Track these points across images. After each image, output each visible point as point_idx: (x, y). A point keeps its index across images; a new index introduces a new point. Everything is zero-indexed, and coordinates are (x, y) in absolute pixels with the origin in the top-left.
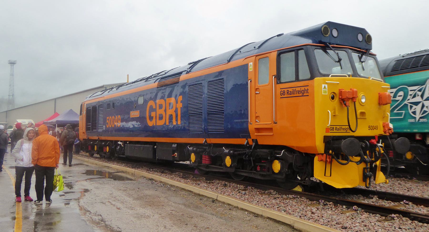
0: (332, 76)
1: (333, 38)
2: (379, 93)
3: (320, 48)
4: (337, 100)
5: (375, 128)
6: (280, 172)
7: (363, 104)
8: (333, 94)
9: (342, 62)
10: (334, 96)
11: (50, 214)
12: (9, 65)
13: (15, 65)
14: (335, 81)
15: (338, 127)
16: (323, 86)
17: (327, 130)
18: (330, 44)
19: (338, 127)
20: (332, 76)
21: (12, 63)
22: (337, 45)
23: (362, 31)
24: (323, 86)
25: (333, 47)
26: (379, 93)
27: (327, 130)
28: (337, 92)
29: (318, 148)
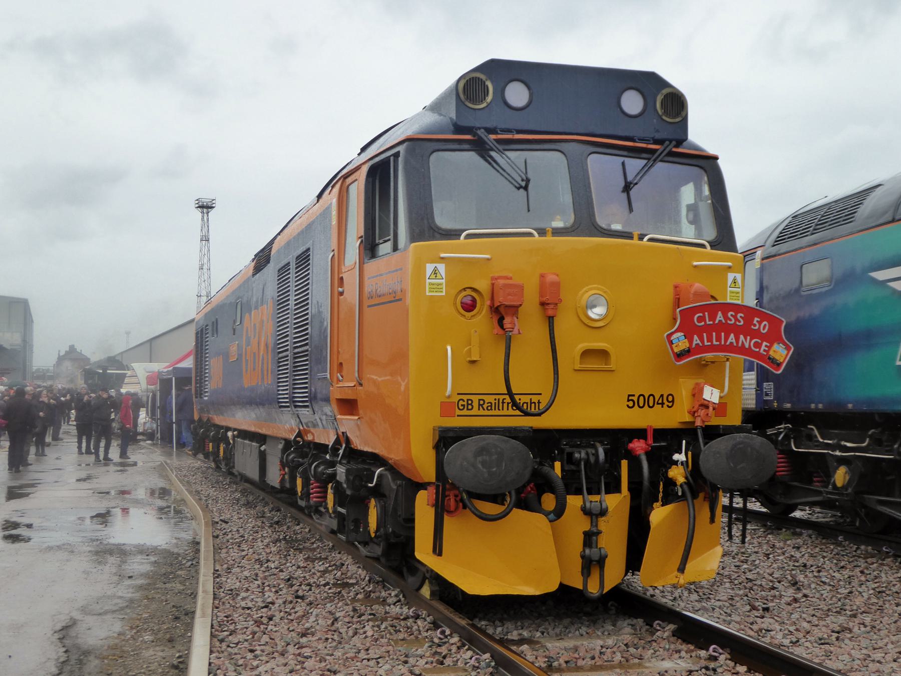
0: (469, 236)
1: (526, 110)
2: (676, 287)
3: (466, 146)
4: (483, 308)
5: (668, 401)
6: (845, 487)
7: (601, 324)
8: (469, 292)
9: (622, 184)
10: (474, 301)
11: (97, 553)
12: (198, 214)
13: (212, 213)
14: (475, 251)
15: (488, 399)
16: (430, 268)
17: (447, 408)
18: (491, 131)
19: (488, 399)
20: (469, 236)
21: (205, 207)
22: (519, 132)
23: (648, 83)
24: (430, 268)
25: (499, 141)
26: (676, 287)
27: (447, 408)
28: (483, 285)
29: (417, 465)
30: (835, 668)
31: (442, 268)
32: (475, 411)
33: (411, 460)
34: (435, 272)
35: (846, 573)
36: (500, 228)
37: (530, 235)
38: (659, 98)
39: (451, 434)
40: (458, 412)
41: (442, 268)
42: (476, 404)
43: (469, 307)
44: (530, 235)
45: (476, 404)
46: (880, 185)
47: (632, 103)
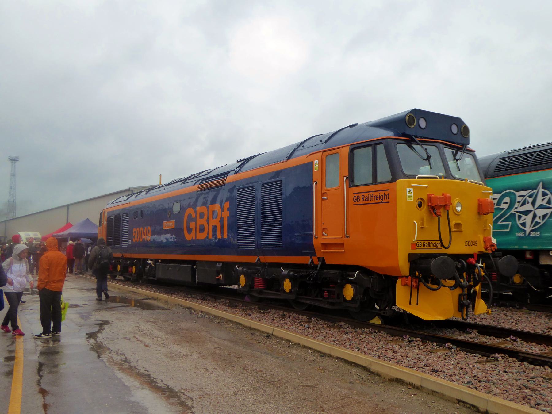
2: (479, 200)
3: (403, 142)
7: (458, 214)
8: (420, 200)
9: (431, 160)
10: (421, 203)
16: (408, 190)
17: (413, 246)
20: (419, 178)
23: (457, 121)
24: (408, 190)
26: (479, 200)
27: (413, 246)
28: (425, 197)
30: (502, 361)
31: (412, 190)
32: (422, 247)
33: (398, 266)
34: (410, 192)
35: (350, 337)
37: (436, 178)
38: (415, 124)
39: (423, 256)
40: (417, 248)
41: (412, 190)
42: (422, 245)
44: (436, 178)
45: (422, 245)
46: (260, 154)
47: (454, 129)
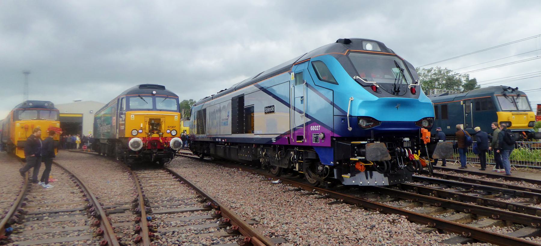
17: (20, 139)
36: (27, 119)
43: (22, 128)
